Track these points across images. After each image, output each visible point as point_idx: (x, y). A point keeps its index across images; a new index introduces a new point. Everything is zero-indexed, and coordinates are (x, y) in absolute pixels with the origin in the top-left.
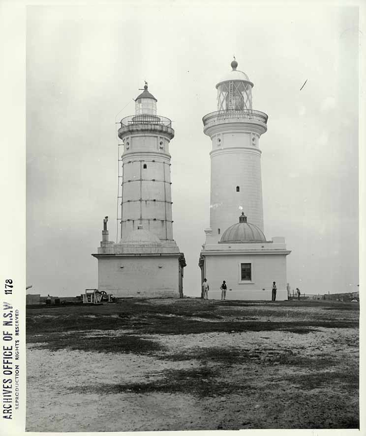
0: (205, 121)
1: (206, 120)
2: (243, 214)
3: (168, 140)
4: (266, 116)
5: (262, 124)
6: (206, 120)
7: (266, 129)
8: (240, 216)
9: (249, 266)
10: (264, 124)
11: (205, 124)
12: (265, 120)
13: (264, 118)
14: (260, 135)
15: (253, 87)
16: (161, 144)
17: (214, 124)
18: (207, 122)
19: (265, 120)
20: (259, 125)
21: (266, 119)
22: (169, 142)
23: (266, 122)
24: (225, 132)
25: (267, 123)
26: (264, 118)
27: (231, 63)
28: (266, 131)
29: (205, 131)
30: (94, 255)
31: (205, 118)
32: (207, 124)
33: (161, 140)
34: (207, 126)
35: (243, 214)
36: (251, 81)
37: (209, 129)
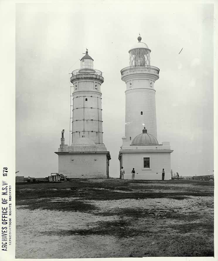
0: (122, 72)
1: (123, 72)
2: (145, 128)
3: (100, 84)
4: (158, 70)
5: (156, 74)
6: (123, 72)
7: (158, 77)
8: (143, 129)
9: (148, 159)
10: (157, 74)
11: (122, 74)
12: (158, 72)
13: (157, 71)
14: (155, 81)
15: (151, 52)
16: (96, 86)
17: (127, 74)
18: (123, 73)
19: (158, 72)
20: (154, 75)
21: (158, 71)
22: (101, 85)
23: (158, 73)
24: (134, 79)
25: (159, 73)
26: (157, 71)
27: (137, 38)
28: (158, 79)
29: (122, 79)
30: (56, 153)
31: (122, 71)
32: (123, 74)
33: (96, 84)
34: (123, 76)
35: (145, 128)
36: (149, 49)
37: (124, 77)
